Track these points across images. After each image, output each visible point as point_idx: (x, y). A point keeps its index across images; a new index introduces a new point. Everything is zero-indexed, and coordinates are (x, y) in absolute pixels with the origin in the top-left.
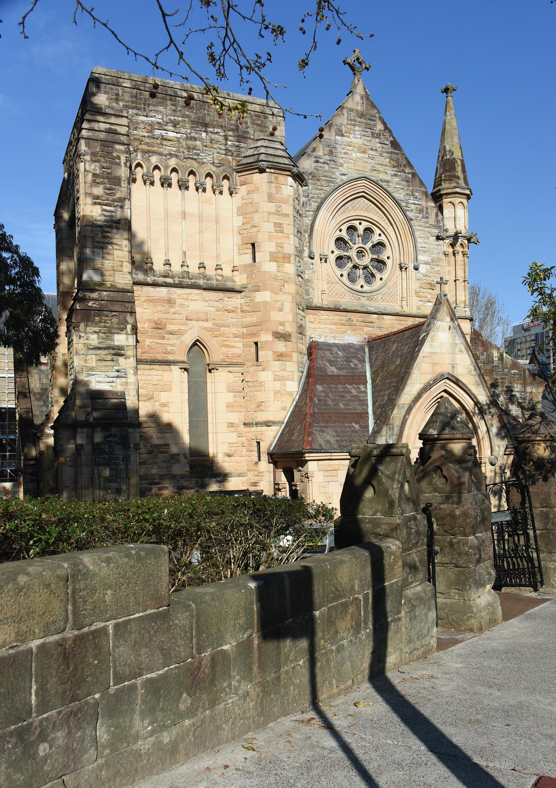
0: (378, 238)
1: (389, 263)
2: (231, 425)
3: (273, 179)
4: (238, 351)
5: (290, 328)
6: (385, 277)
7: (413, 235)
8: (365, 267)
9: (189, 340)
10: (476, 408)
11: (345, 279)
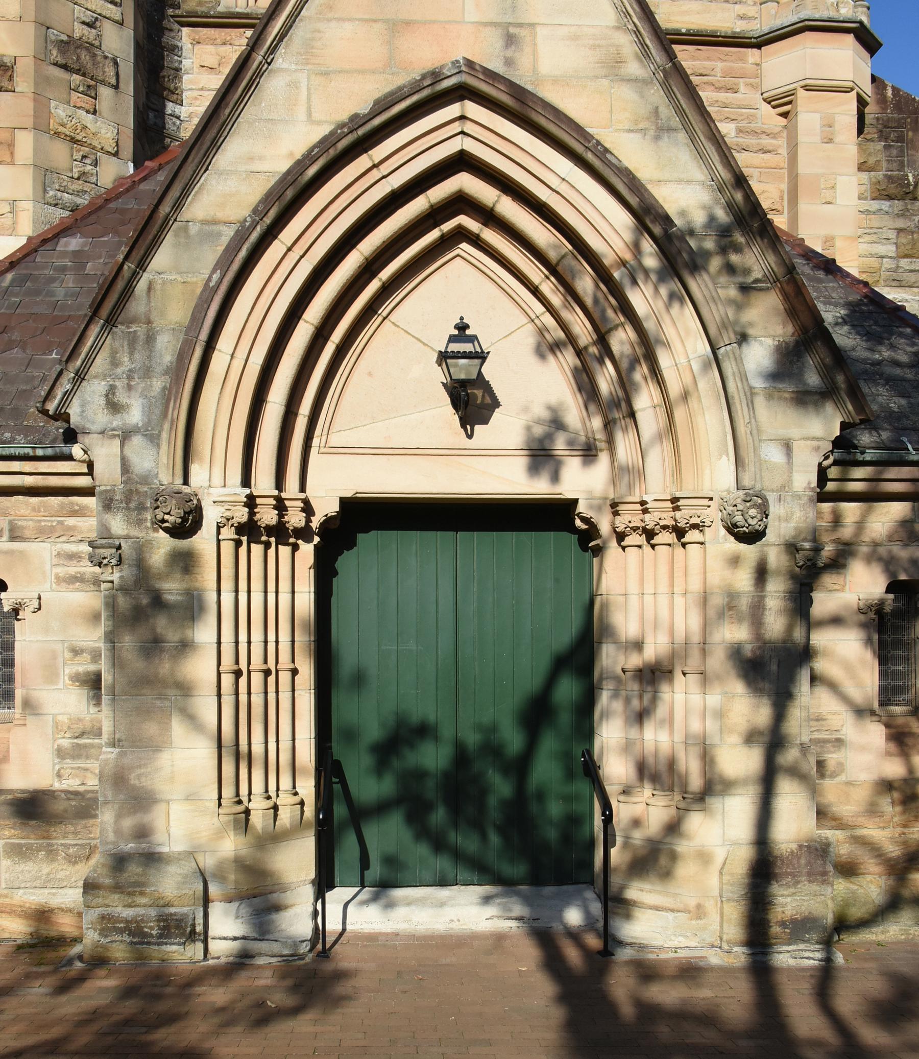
10: (648, 246)
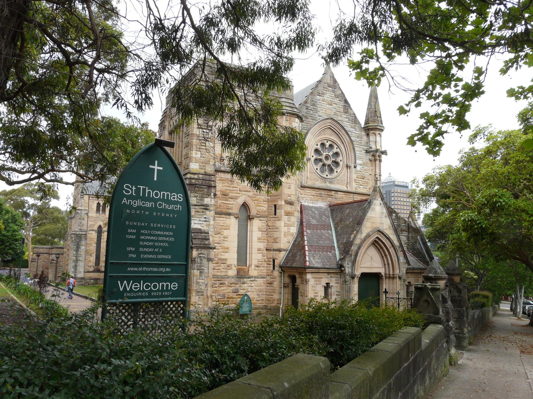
0: (336, 150)
1: (341, 163)
2: (259, 250)
3: (288, 119)
4: (265, 209)
5: (293, 198)
6: (339, 171)
7: (354, 149)
8: (329, 165)
9: (240, 201)
11: (318, 171)
